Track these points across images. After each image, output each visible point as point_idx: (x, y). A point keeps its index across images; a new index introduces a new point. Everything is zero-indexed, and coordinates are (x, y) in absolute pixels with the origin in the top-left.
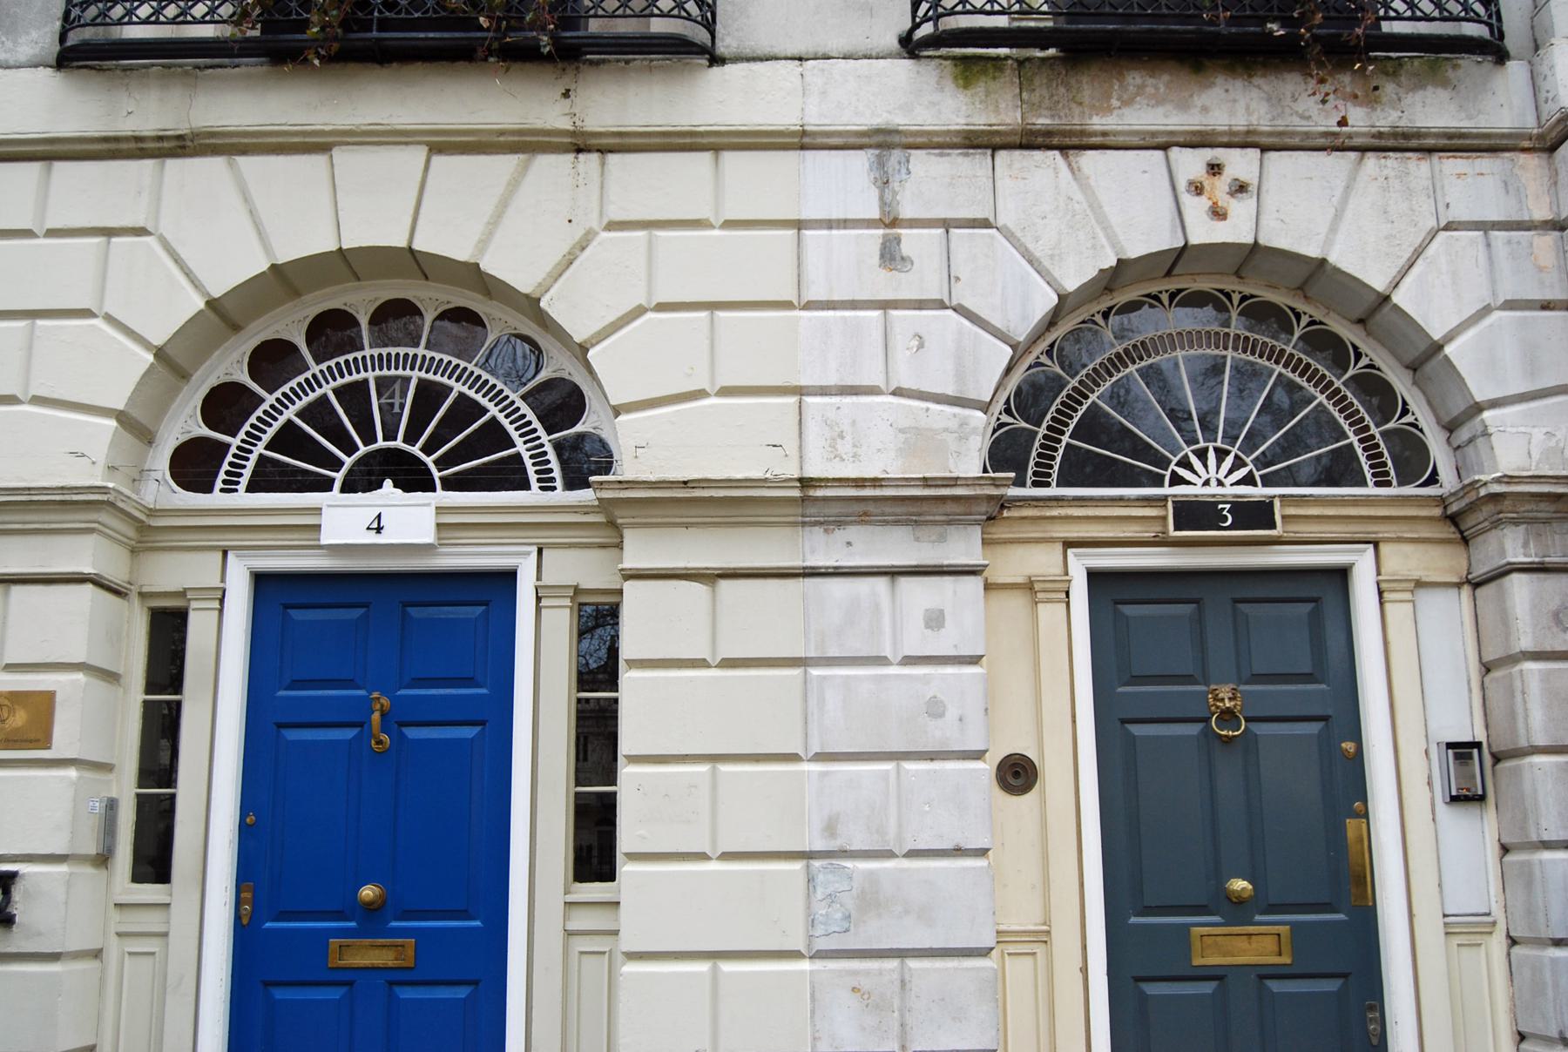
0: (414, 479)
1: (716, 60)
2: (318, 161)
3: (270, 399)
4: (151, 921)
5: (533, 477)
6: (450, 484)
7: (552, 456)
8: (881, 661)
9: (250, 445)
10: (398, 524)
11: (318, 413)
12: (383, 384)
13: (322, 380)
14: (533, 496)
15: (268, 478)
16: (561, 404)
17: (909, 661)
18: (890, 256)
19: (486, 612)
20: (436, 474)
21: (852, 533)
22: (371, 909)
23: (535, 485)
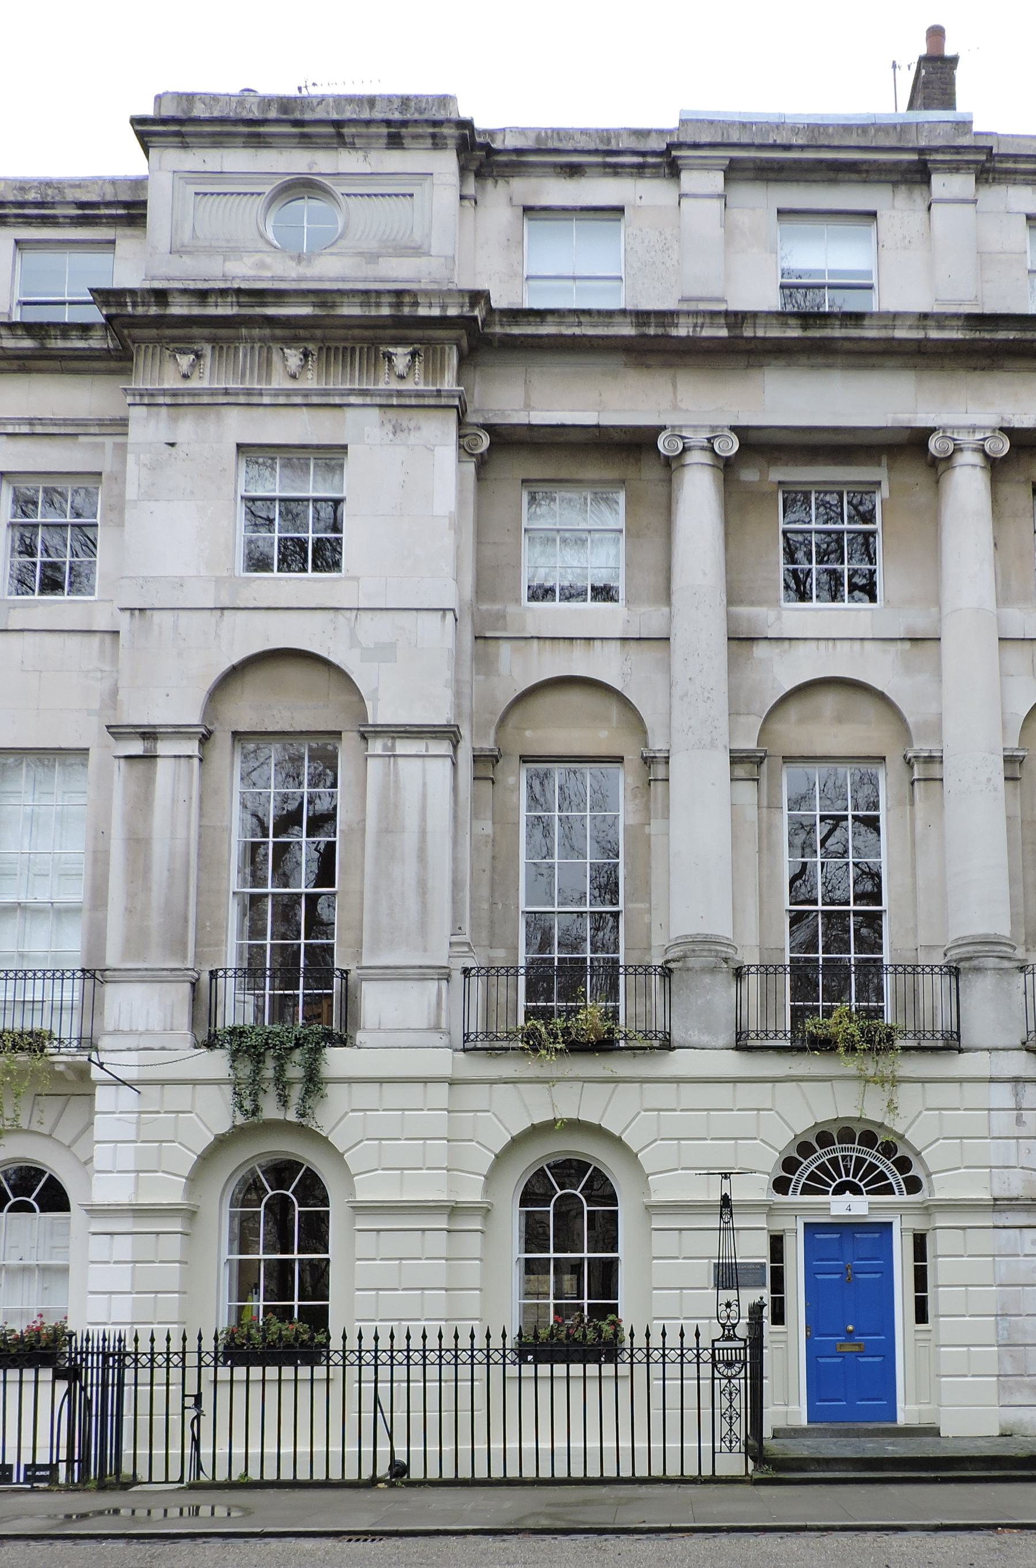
0: (856, 1191)
1: (961, 1051)
2: (829, 1083)
3: (805, 1163)
4: (782, 1338)
5: (896, 1191)
6: (868, 1193)
7: (902, 1183)
8: (1018, 1255)
9: (800, 1178)
10: (853, 1207)
11: (822, 1167)
12: (844, 1158)
13: (822, 1156)
14: (895, 1198)
15: (807, 1190)
16: (904, 1164)
17: (1026, 1255)
18: (1019, 1121)
19: (881, 1237)
20: (864, 1190)
21: (1008, 1214)
22: (851, 1332)
23: (897, 1193)
